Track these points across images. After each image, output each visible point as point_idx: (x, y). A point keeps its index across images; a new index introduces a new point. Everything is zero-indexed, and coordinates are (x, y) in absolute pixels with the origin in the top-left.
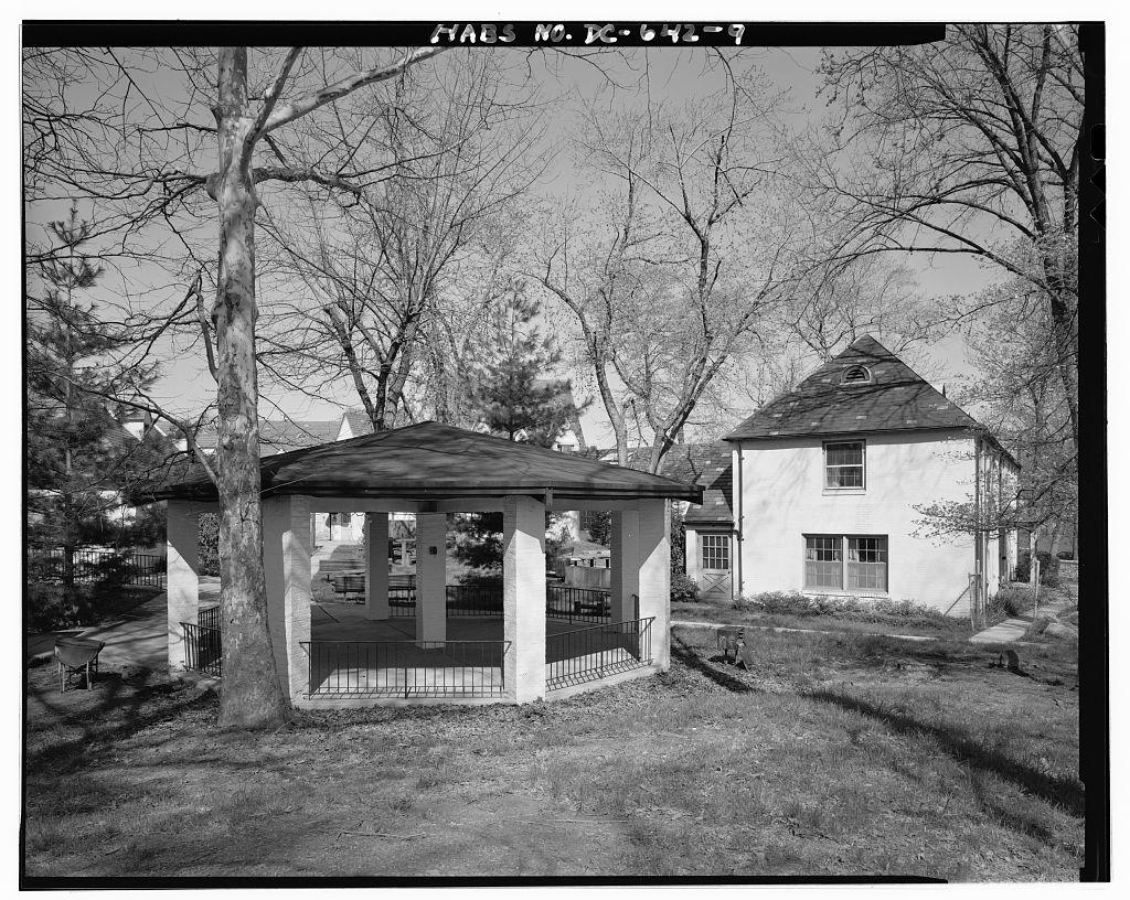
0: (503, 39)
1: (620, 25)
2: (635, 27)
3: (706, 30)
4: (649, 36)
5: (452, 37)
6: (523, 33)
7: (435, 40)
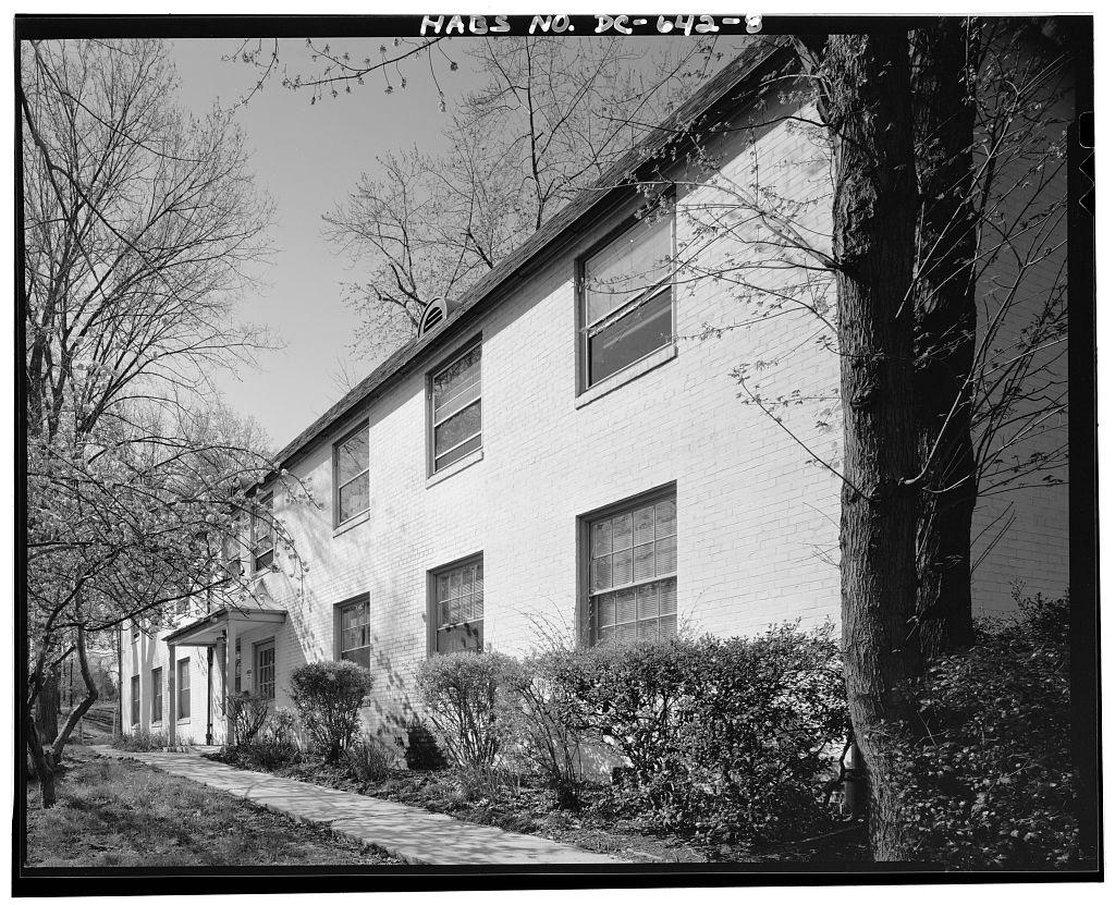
0: (493, 29)
1: (632, 18)
2: (653, 20)
3: (725, 21)
4: (668, 27)
5: (437, 30)
6: (519, 25)
7: (532, 30)
